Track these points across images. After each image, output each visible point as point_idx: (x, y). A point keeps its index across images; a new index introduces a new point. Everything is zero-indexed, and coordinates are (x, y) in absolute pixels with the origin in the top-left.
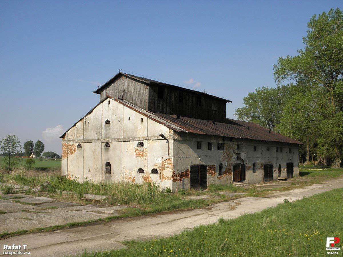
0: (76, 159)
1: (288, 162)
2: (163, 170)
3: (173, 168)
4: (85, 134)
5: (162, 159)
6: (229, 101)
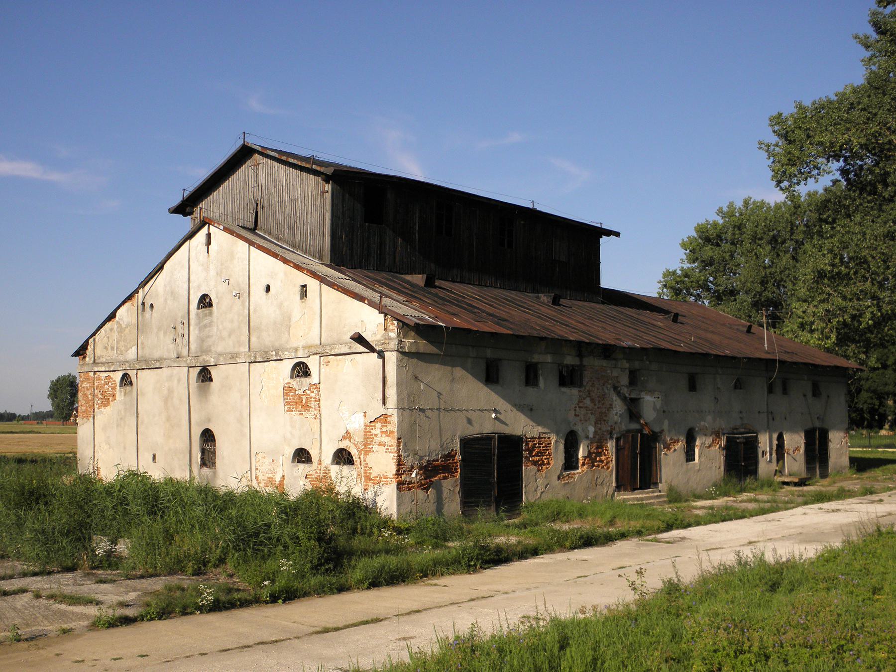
0: (117, 421)
1: (809, 426)
2: (367, 453)
3: (398, 446)
4: (142, 343)
5: (365, 416)
6: (609, 233)
